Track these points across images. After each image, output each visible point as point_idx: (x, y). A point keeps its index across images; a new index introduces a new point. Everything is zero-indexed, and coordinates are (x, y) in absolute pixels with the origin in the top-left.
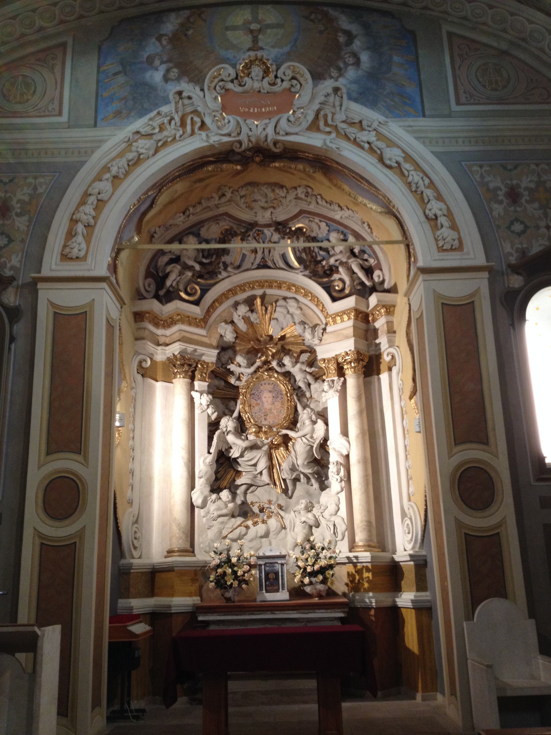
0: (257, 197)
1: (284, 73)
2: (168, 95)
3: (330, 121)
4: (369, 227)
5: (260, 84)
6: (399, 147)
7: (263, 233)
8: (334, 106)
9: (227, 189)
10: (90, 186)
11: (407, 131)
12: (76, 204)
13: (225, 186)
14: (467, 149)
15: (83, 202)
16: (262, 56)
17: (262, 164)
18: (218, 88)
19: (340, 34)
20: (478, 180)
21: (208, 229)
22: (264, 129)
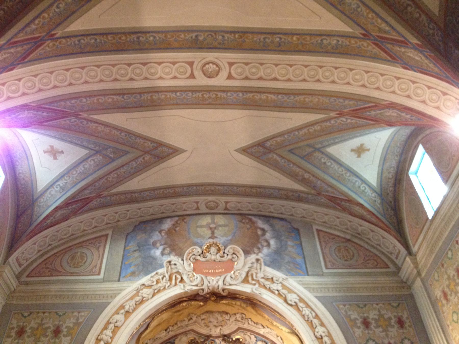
0: (212, 320)
1: (229, 252)
2: (163, 263)
3: (255, 278)
4: (282, 340)
5: (215, 257)
6: (295, 293)
7: (215, 342)
8: (257, 269)
9: (193, 315)
10: (111, 317)
11: (299, 284)
12: (101, 329)
13: (192, 313)
14: (335, 294)
15: (105, 328)
16: (217, 242)
17: (215, 301)
18: (191, 259)
19: (258, 230)
20: (344, 313)
21: (180, 340)
22: (217, 282)
